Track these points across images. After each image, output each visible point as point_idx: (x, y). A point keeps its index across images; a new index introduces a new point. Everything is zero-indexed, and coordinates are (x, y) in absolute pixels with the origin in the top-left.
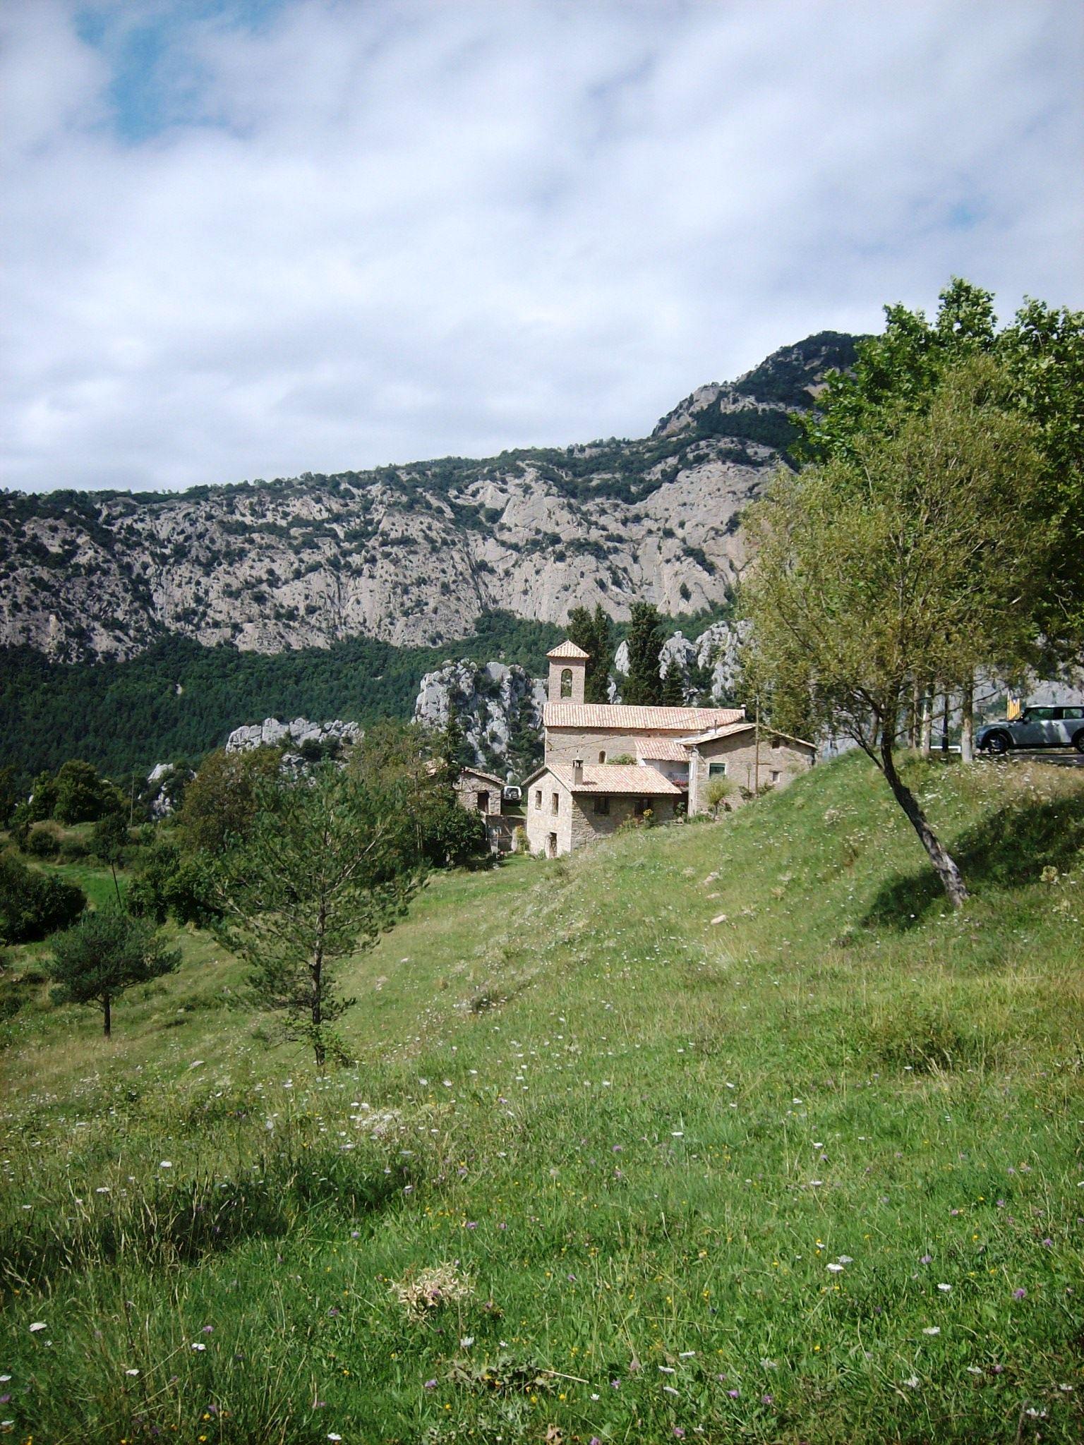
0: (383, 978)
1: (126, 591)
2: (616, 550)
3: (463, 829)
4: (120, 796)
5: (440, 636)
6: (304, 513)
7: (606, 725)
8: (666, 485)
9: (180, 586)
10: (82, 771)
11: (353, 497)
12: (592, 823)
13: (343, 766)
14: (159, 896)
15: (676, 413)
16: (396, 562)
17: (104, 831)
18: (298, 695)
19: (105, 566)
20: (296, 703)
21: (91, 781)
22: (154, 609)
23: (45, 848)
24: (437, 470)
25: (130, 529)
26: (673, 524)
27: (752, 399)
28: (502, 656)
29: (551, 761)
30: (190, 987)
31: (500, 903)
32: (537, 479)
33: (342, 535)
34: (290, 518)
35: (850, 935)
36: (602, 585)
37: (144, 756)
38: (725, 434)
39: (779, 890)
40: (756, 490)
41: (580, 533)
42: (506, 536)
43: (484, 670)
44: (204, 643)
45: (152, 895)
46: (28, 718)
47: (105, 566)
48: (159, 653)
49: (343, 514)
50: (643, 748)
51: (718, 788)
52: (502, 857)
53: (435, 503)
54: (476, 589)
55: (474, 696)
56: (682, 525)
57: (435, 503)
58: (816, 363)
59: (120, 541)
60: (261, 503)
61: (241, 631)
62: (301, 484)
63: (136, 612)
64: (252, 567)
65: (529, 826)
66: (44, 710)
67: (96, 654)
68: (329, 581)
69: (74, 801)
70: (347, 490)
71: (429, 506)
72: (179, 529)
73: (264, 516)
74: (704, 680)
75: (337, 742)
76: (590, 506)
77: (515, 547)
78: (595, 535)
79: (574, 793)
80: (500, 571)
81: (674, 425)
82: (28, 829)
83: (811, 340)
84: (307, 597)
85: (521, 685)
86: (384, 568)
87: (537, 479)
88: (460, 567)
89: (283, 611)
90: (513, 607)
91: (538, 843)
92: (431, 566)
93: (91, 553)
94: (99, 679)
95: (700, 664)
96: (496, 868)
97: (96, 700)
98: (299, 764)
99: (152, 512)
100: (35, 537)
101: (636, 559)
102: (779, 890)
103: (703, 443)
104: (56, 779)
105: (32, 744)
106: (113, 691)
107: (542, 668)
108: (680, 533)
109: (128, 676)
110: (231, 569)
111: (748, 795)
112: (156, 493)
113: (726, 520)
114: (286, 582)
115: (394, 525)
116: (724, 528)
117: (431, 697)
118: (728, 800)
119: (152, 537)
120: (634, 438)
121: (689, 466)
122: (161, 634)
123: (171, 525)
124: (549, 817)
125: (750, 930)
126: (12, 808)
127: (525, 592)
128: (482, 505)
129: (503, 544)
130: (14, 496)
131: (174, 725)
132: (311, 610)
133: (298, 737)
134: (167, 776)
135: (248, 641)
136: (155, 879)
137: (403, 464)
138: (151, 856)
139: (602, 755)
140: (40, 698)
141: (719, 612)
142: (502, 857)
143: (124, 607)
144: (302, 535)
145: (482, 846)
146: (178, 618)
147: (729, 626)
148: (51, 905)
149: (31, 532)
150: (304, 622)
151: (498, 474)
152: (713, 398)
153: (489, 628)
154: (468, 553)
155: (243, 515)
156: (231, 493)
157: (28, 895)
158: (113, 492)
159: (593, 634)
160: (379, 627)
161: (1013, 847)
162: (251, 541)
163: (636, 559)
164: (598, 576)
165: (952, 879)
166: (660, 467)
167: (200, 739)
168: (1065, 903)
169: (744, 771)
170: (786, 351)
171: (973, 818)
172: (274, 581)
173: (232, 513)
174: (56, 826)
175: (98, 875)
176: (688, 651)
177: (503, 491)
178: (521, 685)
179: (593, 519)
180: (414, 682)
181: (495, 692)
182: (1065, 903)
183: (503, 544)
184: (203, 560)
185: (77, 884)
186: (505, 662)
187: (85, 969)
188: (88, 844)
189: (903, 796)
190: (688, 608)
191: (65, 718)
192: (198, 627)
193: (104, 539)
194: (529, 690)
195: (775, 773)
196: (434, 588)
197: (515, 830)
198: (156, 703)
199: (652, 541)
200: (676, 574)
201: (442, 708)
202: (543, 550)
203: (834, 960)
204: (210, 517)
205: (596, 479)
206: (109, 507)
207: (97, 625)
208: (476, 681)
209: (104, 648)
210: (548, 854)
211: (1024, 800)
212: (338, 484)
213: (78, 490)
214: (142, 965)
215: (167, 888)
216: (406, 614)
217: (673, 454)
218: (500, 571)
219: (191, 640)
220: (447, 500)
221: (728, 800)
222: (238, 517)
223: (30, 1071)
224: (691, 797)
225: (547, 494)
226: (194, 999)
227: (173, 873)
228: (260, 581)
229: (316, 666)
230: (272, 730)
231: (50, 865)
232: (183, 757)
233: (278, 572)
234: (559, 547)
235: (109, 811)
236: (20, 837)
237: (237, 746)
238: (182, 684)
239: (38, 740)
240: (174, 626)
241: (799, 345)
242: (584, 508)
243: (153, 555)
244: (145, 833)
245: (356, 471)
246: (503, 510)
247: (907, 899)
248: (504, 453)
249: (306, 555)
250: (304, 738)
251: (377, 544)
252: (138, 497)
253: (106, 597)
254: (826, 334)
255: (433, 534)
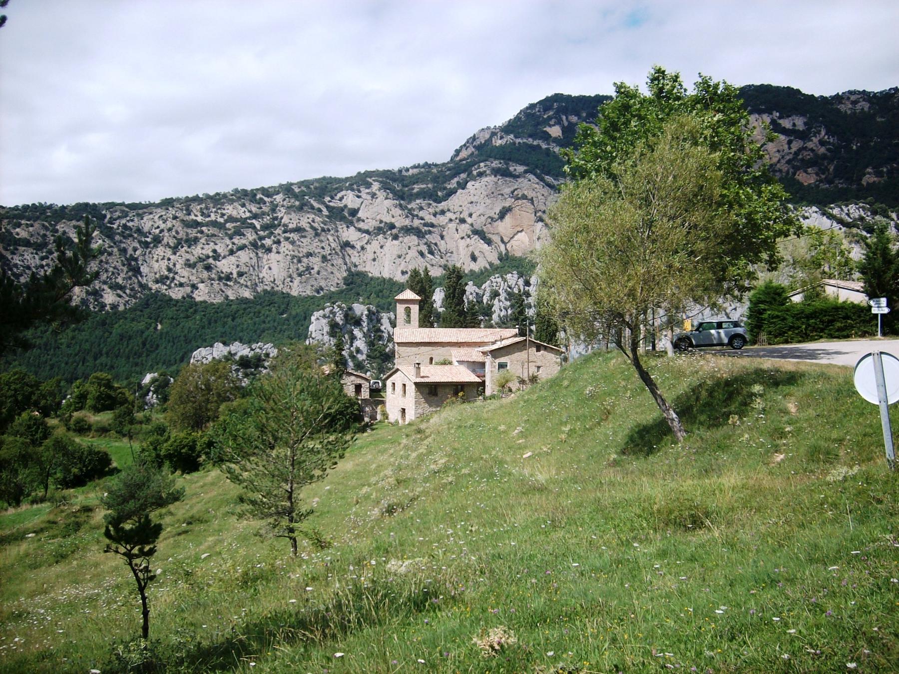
0: (317, 499)
1: (124, 265)
2: (430, 232)
3: (347, 408)
4: (127, 394)
5: (322, 289)
6: (234, 214)
7: (433, 341)
8: (460, 191)
9: (157, 261)
10: (102, 379)
11: (265, 203)
12: (427, 401)
13: (264, 371)
14: (158, 456)
15: (465, 146)
16: (293, 243)
17: (120, 416)
18: (234, 328)
19: (110, 250)
20: (233, 332)
21: (108, 385)
22: (142, 276)
23: (82, 428)
24: (317, 185)
25: (125, 227)
26: (465, 215)
27: (512, 136)
28: (361, 300)
29: (400, 364)
30: (188, 510)
31: (379, 451)
32: (380, 189)
33: (258, 227)
34: (226, 217)
35: (615, 460)
36: (422, 254)
37: (138, 369)
38: (496, 159)
39: (563, 436)
40: (516, 193)
41: (407, 222)
42: (361, 225)
43: (350, 309)
44: (174, 296)
45: (154, 455)
46: (63, 347)
47: (110, 250)
48: (146, 304)
49: (256, 214)
50: (456, 354)
51: (504, 378)
52: (372, 424)
53: (316, 205)
54: (344, 259)
55: (344, 325)
56: (470, 215)
57: (316, 205)
58: (551, 113)
59: (119, 234)
60: (207, 208)
61: (197, 288)
62: (232, 195)
63: (130, 278)
64: (203, 248)
65: (387, 404)
66: (73, 342)
67: (106, 306)
68: (252, 256)
69: (98, 399)
70: (261, 199)
71: (313, 208)
72: (156, 226)
73: (209, 216)
74: (488, 312)
75: (260, 356)
76: (413, 205)
77: (367, 232)
78: (417, 223)
79: (416, 384)
80: (358, 247)
81: (464, 154)
82: (71, 416)
83: (547, 99)
84: (238, 266)
85: (374, 318)
86: (285, 247)
87: (380, 189)
88: (333, 245)
89: (223, 275)
90: (367, 269)
91: (394, 415)
92: (315, 245)
93: (100, 242)
94: (108, 321)
95: (485, 301)
96: (369, 431)
97: (106, 334)
98: (237, 370)
99: (138, 215)
100: (64, 233)
101: (442, 237)
102: (563, 436)
103: (482, 164)
104: (87, 385)
105: (67, 363)
106: (117, 329)
107: (386, 307)
108: (469, 220)
109: (126, 318)
110: (189, 250)
111: (522, 382)
112: (140, 203)
113: (498, 212)
114: (224, 257)
115: (290, 220)
116: (496, 216)
117: (318, 327)
118: (510, 385)
119: (139, 231)
120: (439, 162)
121: (474, 179)
122: (146, 292)
123: (151, 223)
124: (400, 398)
125: (548, 460)
126: (60, 403)
127: (374, 260)
128: (346, 206)
129: (360, 230)
130: (50, 207)
131: (157, 349)
132: (240, 274)
133: (235, 354)
134: (154, 381)
135: (201, 295)
136: (155, 446)
137: (295, 182)
138: (151, 431)
139: (431, 359)
140: (71, 334)
141: (493, 270)
142: (372, 424)
143: (123, 275)
144: (234, 227)
145: (359, 418)
146: (157, 282)
147: (502, 277)
148: (89, 464)
149: (61, 230)
150: (236, 282)
151: (355, 187)
152: (487, 136)
153: (352, 283)
154: (338, 237)
155: (196, 216)
156: (188, 203)
157: (75, 458)
158: (113, 203)
159: (422, 284)
160: (283, 283)
161: (708, 404)
162: (202, 232)
163: (442, 237)
164: (420, 248)
165: (676, 423)
166: (456, 180)
167: (173, 357)
168: (746, 436)
169: (519, 367)
170: (532, 106)
171: (683, 387)
172: (217, 256)
173: (189, 214)
174: (88, 414)
175: (117, 444)
176: (477, 294)
177: (359, 197)
178: (374, 317)
179: (415, 213)
180: (306, 318)
181: (358, 322)
182: (746, 436)
183: (360, 230)
184: (172, 245)
185: (105, 450)
186: (362, 303)
187: (125, 501)
188: (109, 425)
189: (645, 376)
190: (476, 267)
191: (87, 346)
192: (170, 287)
193: (109, 233)
194: (379, 321)
195: (539, 367)
196: (317, 259)
197: (379, 407)
198: (145, 335)
199: (453, 226)
200: (467, 246)
201: (325, 333)
202: (384, 233)
203: (610, 475)
204: (175, 218)
205: (417, 188)
206: (111, 212)
207: (106, 287)
208: (346, 316)
209: (110, 302)
210: (400, 421)
211: (712, 377)
212: (255, 195)
213: (91, 202)
214: (161, 498)
215: (163, 451)
216: (300, 275)
217: (464, 172)
218: (358, 247)
219: (165, 295)
220: (324, 203)
221: (510, 385)
222: (193, 217)
223: (96, 565)
224: (487, 383)
225: (386, 198)
226: (192, 517)
227: (166, 441)
228: (208, 257)
229: (245, 309)
230: (219, 350)
231: (86, 439)
232: (163, 369)
233: (219, 251)
234: (394, 231)
235: (122, 404)
236: (66, 422)
237: (198, 361)
238: (161, 323)
239: (71, 361)
240: (154, 287)
241: (540, 102)
242: (409, 207)
243: (140, 242)
244: (145, 417)
245: (266, 186)
246: (359, 209)
247: (647, 437)
248: (359, 173)
249: (236, 240)
250: (239, 354)
251: (280, 232)
252: (128, 206)
253: (111, 269)
254: (556, 95)
255: (316, 225)
